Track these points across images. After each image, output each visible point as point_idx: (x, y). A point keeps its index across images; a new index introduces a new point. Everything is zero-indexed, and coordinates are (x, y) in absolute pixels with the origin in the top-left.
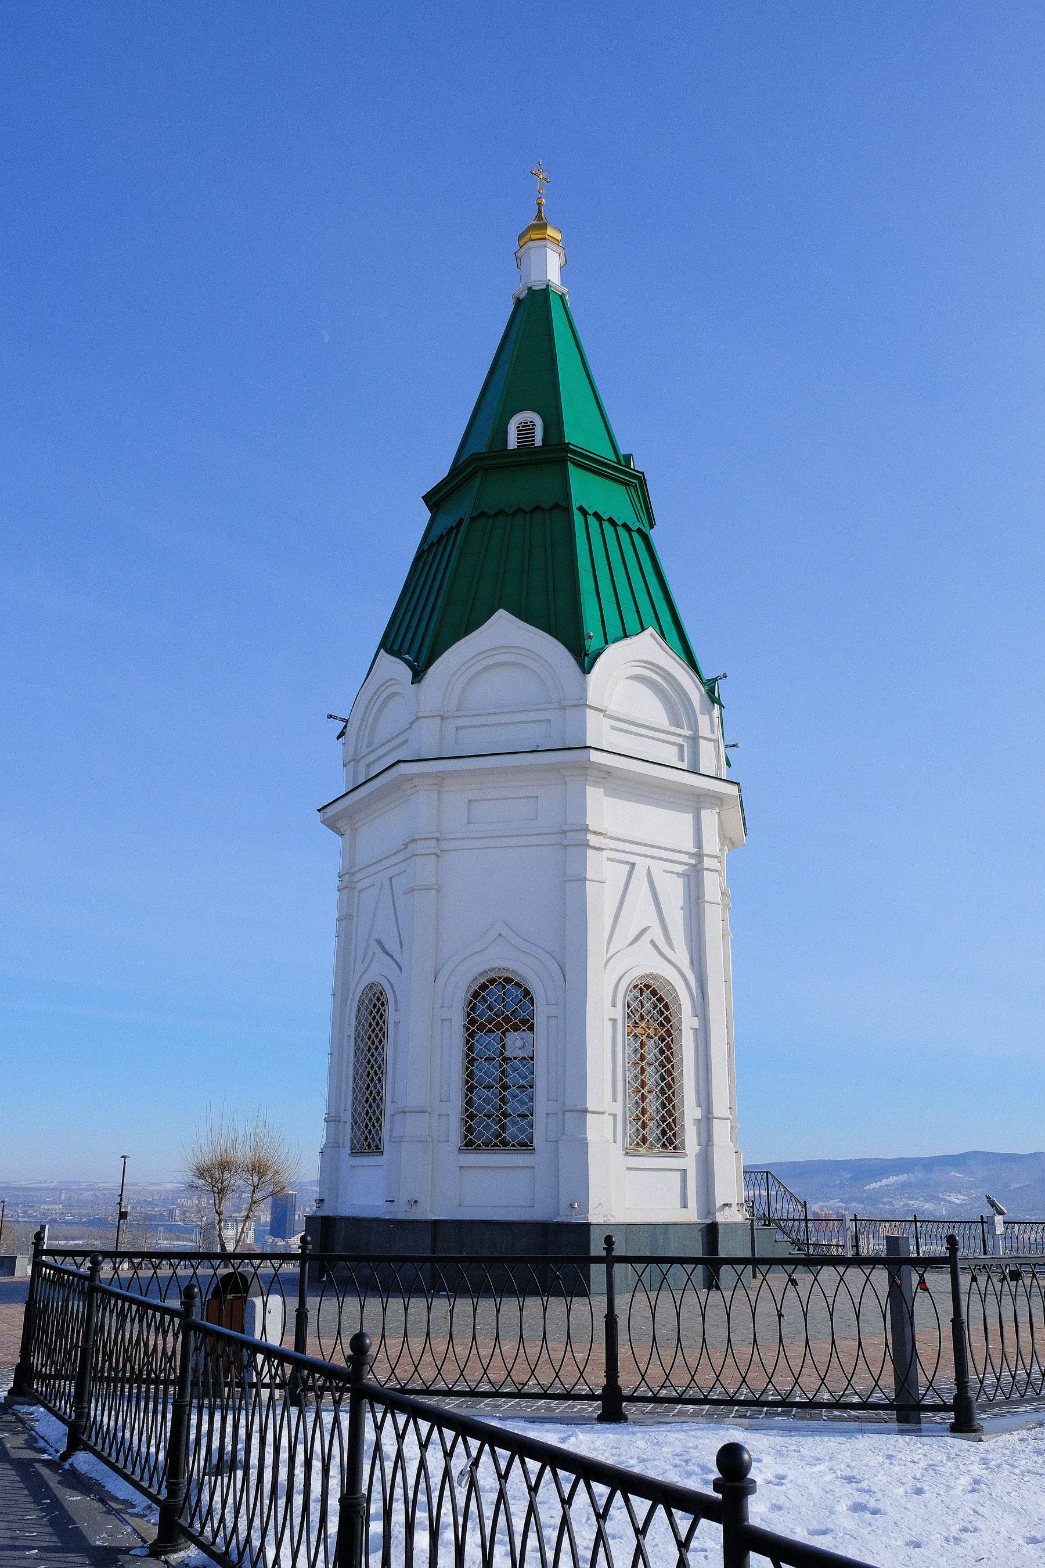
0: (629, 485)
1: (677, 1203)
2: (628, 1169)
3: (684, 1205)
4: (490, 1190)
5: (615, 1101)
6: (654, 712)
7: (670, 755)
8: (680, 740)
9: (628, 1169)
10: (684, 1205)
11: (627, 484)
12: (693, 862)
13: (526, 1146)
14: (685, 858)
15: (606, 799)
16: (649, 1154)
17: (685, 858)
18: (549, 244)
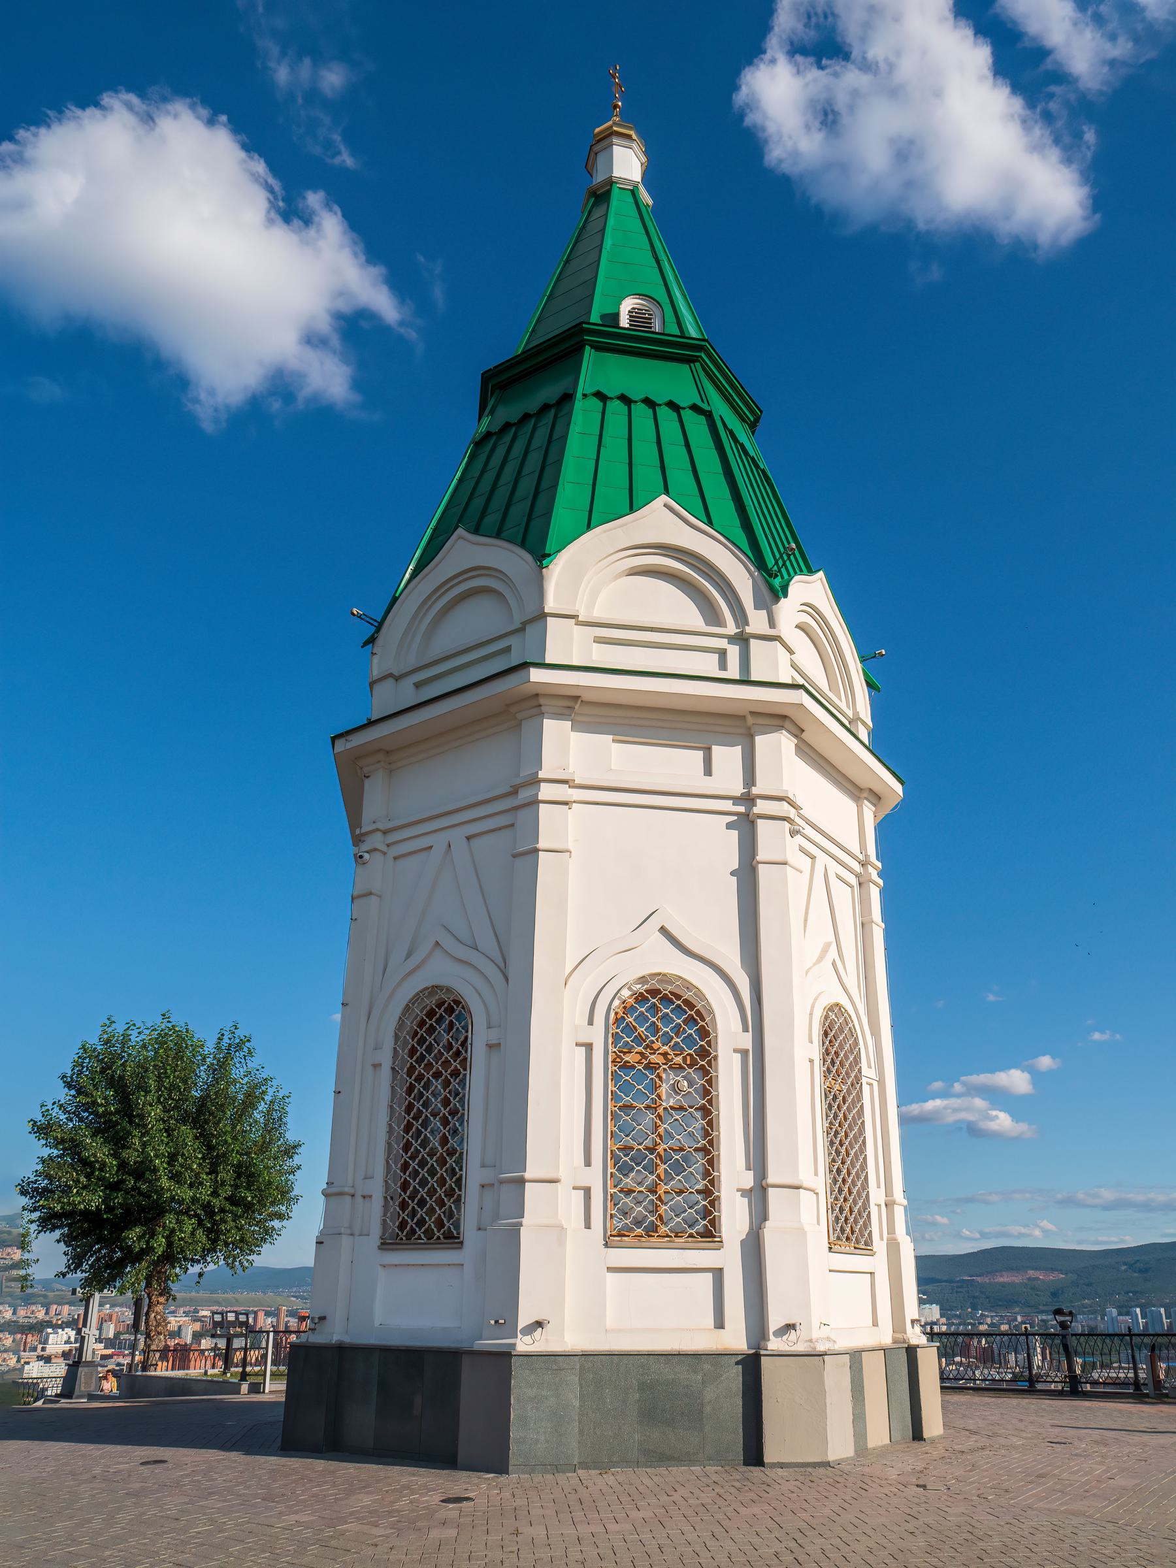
0: (694, 362)
1: (710, 1321)
2: (610, 1269)
3: (720, 1324)
4: (405, 1301)
5: (588, 1163)
6: (674, 607)
7: (708, 665)
8: (723, 643)
9: (610, 1269)
10: (720, 1324)
11: (689, 360)
12: (742, 809)
13: (453, 1239)
14: (728, 805)
15: (616, 747)
16: (639, 1244)
17: (728, 805)
18: (615, 140)
